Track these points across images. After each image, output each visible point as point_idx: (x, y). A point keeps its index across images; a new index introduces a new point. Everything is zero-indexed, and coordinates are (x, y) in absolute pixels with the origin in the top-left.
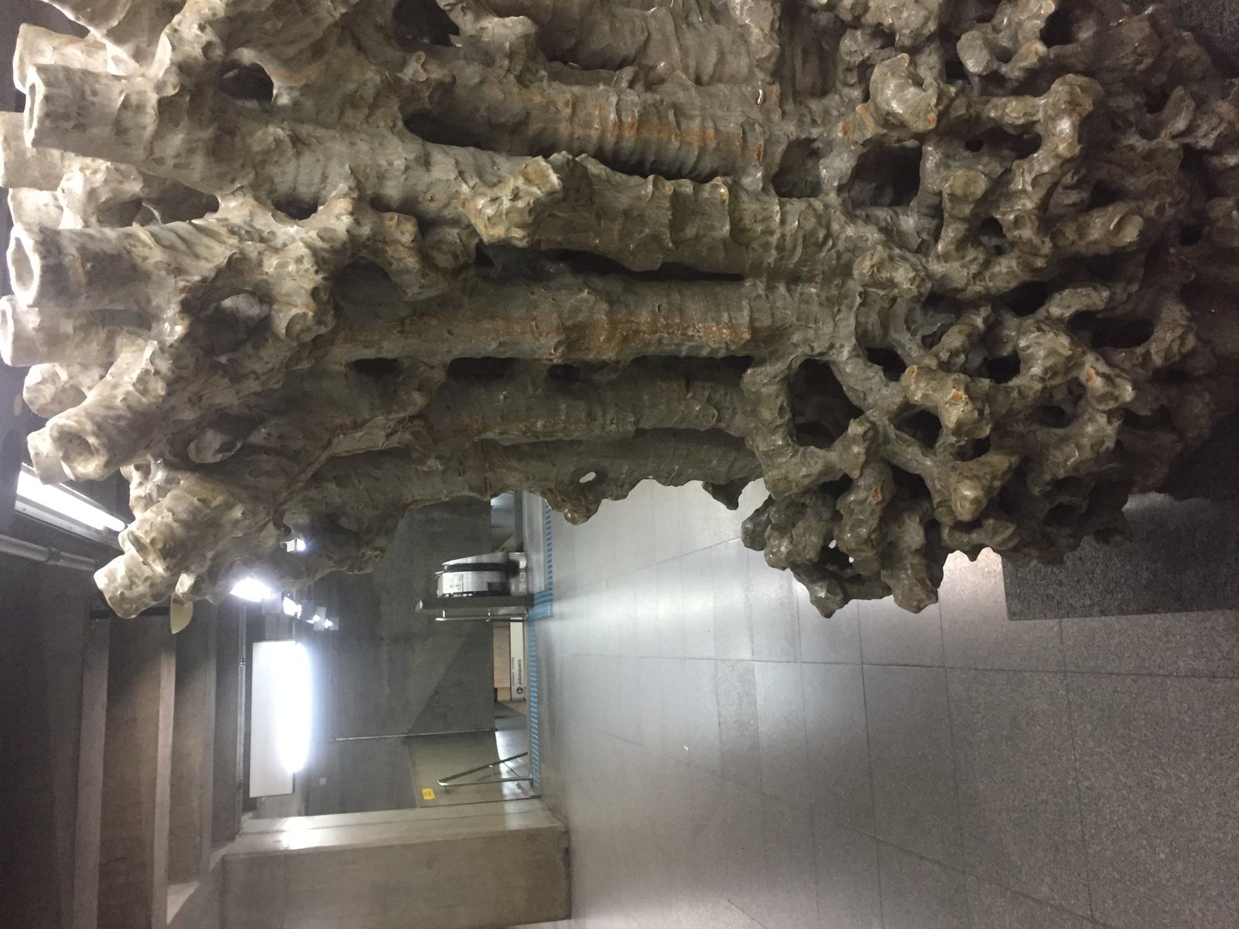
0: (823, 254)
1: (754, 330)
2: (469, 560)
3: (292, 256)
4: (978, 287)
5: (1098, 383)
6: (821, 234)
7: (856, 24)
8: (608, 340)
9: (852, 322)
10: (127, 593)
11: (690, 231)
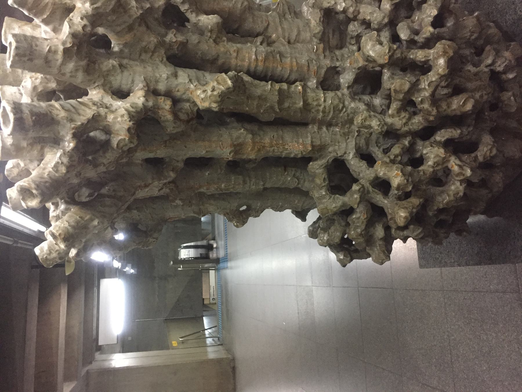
0: (341, 115)
1: (313, 146)
2: (192, 244)
3: (119, 114)
4: (406, 129)
5: (456, 169)
6: (341, 106)
7: (355, 19)
8: (252, 150)
9: (354, 143)
10: (48, 257)
11: (286, 105)
